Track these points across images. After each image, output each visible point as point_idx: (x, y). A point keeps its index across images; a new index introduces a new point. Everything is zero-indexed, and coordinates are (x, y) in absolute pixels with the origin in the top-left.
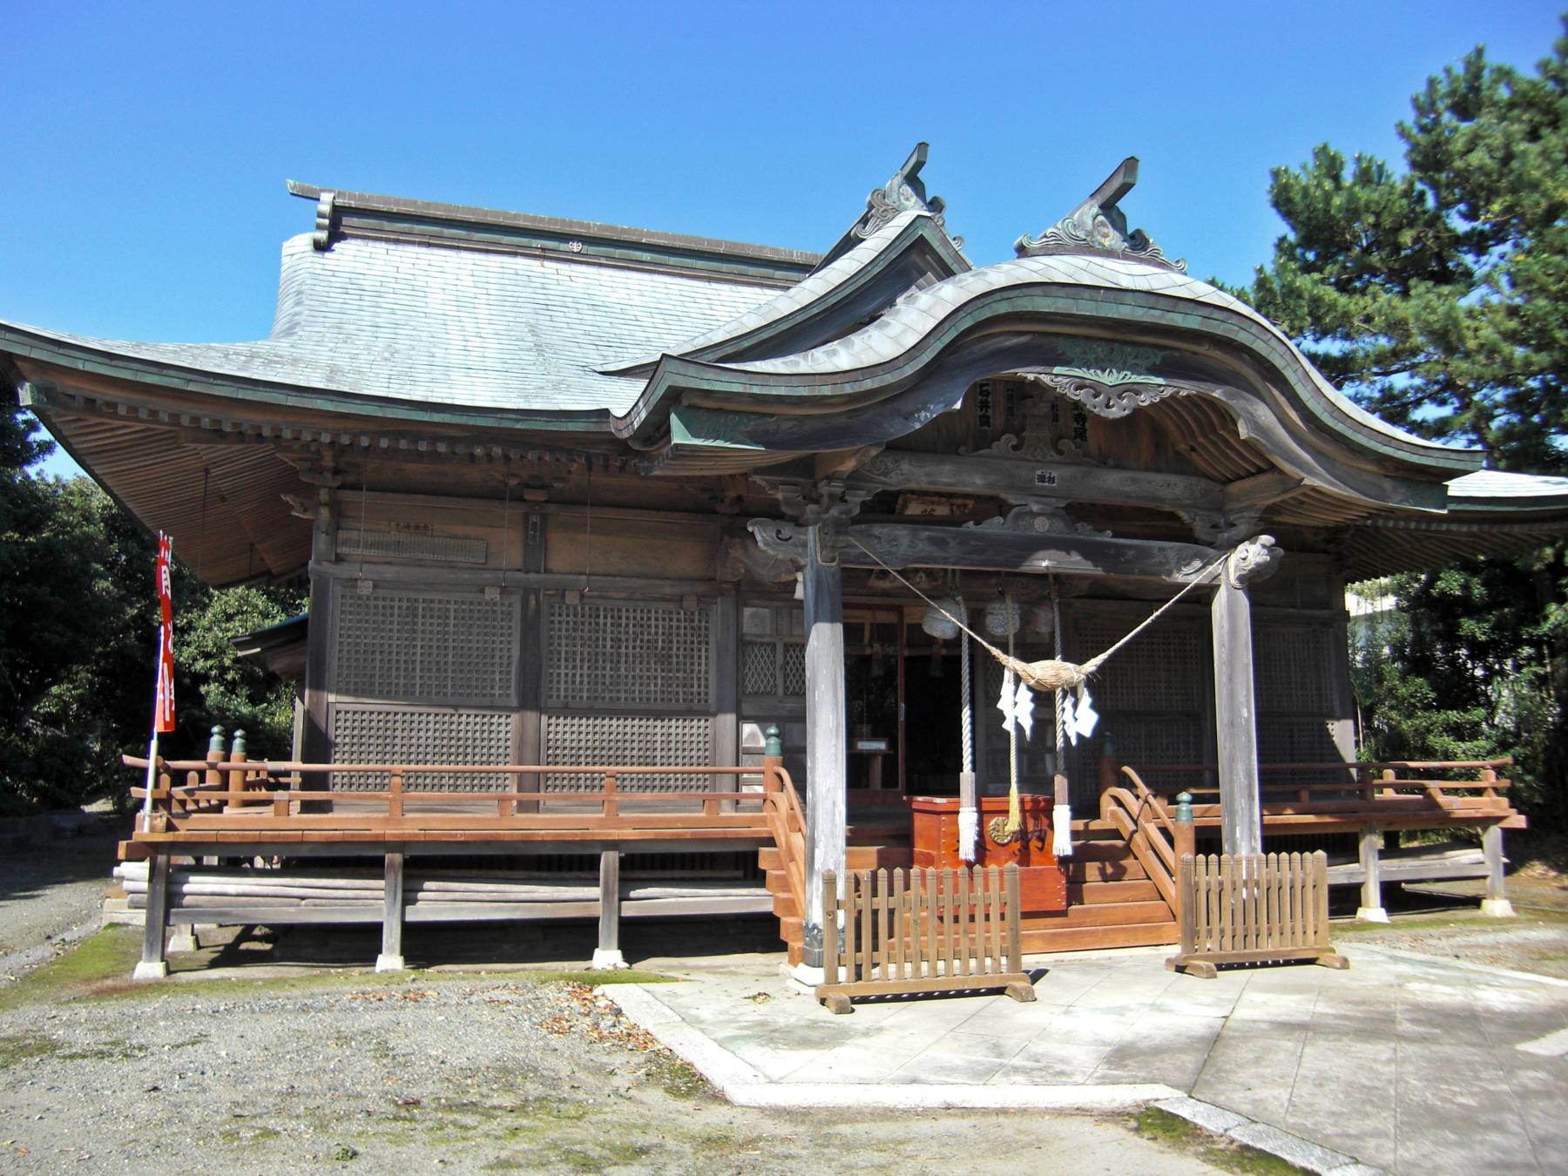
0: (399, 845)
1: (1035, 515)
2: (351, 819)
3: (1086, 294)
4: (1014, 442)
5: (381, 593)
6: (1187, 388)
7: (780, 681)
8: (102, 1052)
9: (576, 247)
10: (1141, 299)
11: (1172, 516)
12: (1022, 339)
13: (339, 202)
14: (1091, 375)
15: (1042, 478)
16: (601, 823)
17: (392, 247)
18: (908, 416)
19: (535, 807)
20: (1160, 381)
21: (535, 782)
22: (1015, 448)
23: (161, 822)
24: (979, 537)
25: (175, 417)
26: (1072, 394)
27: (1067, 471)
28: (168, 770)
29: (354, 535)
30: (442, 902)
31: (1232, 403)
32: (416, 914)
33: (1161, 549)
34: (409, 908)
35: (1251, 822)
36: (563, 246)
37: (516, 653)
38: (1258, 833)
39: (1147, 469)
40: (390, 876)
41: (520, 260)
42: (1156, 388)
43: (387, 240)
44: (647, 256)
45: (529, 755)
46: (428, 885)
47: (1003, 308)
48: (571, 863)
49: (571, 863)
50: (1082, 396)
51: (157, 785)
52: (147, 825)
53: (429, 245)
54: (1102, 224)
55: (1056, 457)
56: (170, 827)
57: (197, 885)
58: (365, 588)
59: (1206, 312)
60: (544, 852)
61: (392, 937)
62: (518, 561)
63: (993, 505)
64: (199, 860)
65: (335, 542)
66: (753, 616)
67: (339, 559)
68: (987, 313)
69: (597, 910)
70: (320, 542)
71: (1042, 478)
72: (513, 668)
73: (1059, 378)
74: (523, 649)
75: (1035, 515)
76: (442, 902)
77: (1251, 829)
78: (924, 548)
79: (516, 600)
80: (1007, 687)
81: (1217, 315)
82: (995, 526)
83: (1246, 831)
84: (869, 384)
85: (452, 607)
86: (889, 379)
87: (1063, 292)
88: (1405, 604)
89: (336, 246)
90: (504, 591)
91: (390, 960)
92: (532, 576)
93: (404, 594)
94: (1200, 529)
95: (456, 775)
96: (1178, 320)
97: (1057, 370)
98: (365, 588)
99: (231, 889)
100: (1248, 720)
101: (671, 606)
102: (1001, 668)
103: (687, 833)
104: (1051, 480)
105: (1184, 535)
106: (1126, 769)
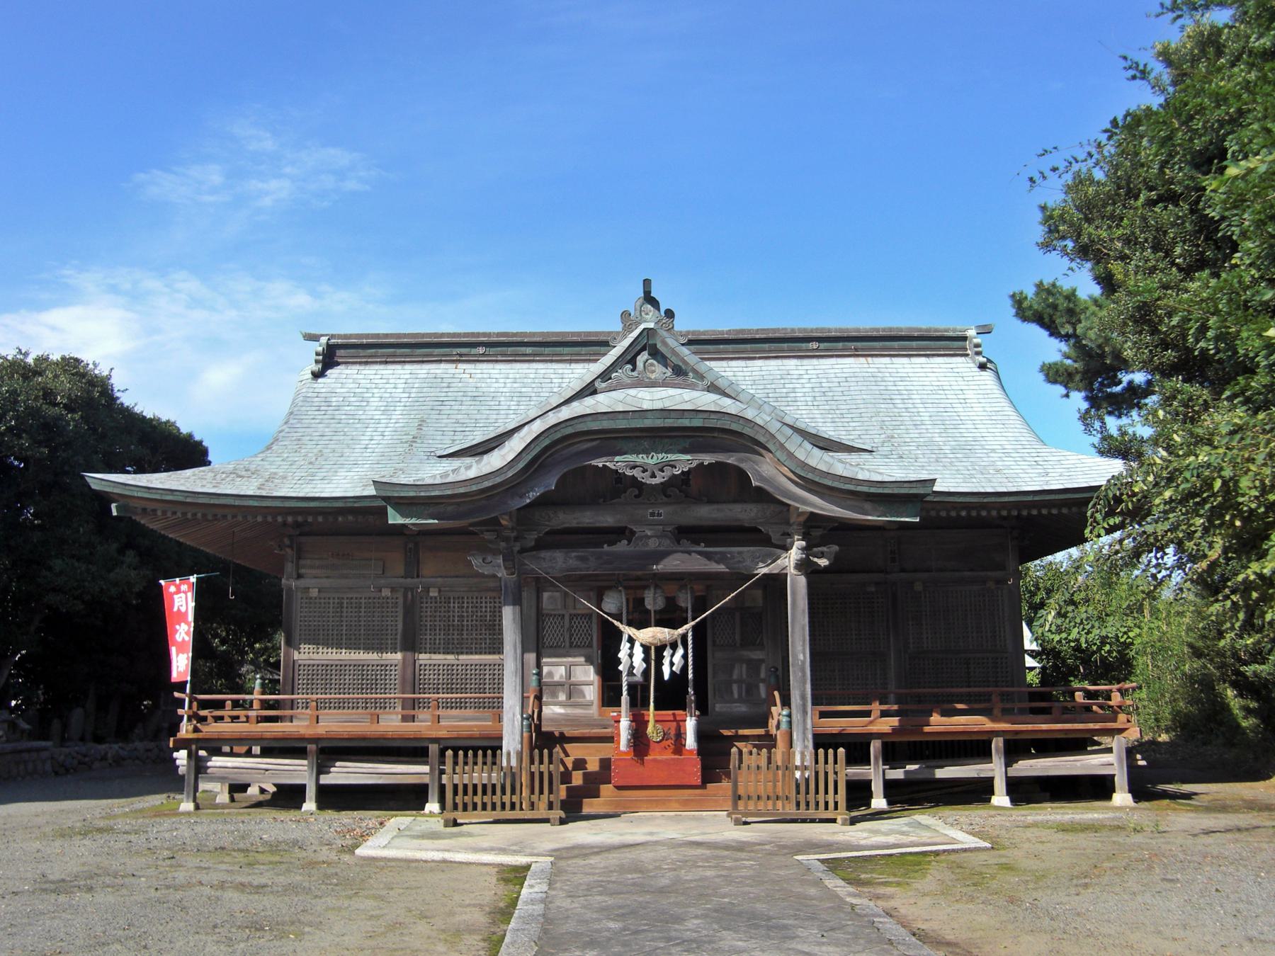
0: (315, 740)
1: (649, 537)
2: (299, 725)
5: (323, 595)
6: (708, 459)
9: (481, 350)
10: (658, 415)
11: (755, 530)
12: (594, 443)
14: (640, 459)
15: (652, 514)
16: (429, 728)
17: (362, 367)
18: (522, 496)
19: (413, 719)
20: (689, 457)
21: (414, 704)
23: (191, 728)
24: (608, 554)
26: (629, 473)
27: (670, 509)
28: (196, 699)
29: (308, 562)
30: (345, 773)
31: (743, 466)
32: (325, 780)
33: (739, 553)
34: (322, 776)
35: (805, 729)
36: (474, 351)
37: (400, 627)
39: (735, 501)
40: (310, 758)
41: (443, 366)
42: (684, 461)
43: (360, 363)
44: (529, 350)
45: (409, 688)
46: (338, 764)
47: (569, 431)
48: (412, 751)
49: (412, 751)
50: (637, 473)
51: (190, 707)
52: (185, 730)
53: (386, 362)
54: (652, 365)
56: (196, 730)
57: (217, 761)
58: (314, 593)
61: (311, 792)
62: (402, 572)
63: (620, 533)
65: (298, 567)
66: (550, 597)
67: (299, 576)
68: (558, 435)
69: (426, 780)
70: (289, 567)
71: (652, 514)
72: (399, 637)
73: (619, 463)
74: (405, 623)
75: (649, 537)
76: (345, 773)
77: (804, 733)
78: (573, 563)
79: (400, 595)
80: (625, 647)
82: (622, 546)
83: (801, 736)
84: (487, 484)
85: (363, 601)
86: (498, 480)
87: (605, 417)
90: (393, 590)
91: (310, 805)
92: (409, 580)
93: (336, 595)
94: (775, 538)
96: (686, 423)
97: (617, 458)
98: (314, 593)
99: (229, 765)
100: (803, 662)
101: (494, 594)
104: (659, 515)
105: (766, 541)
106: (776, 693)
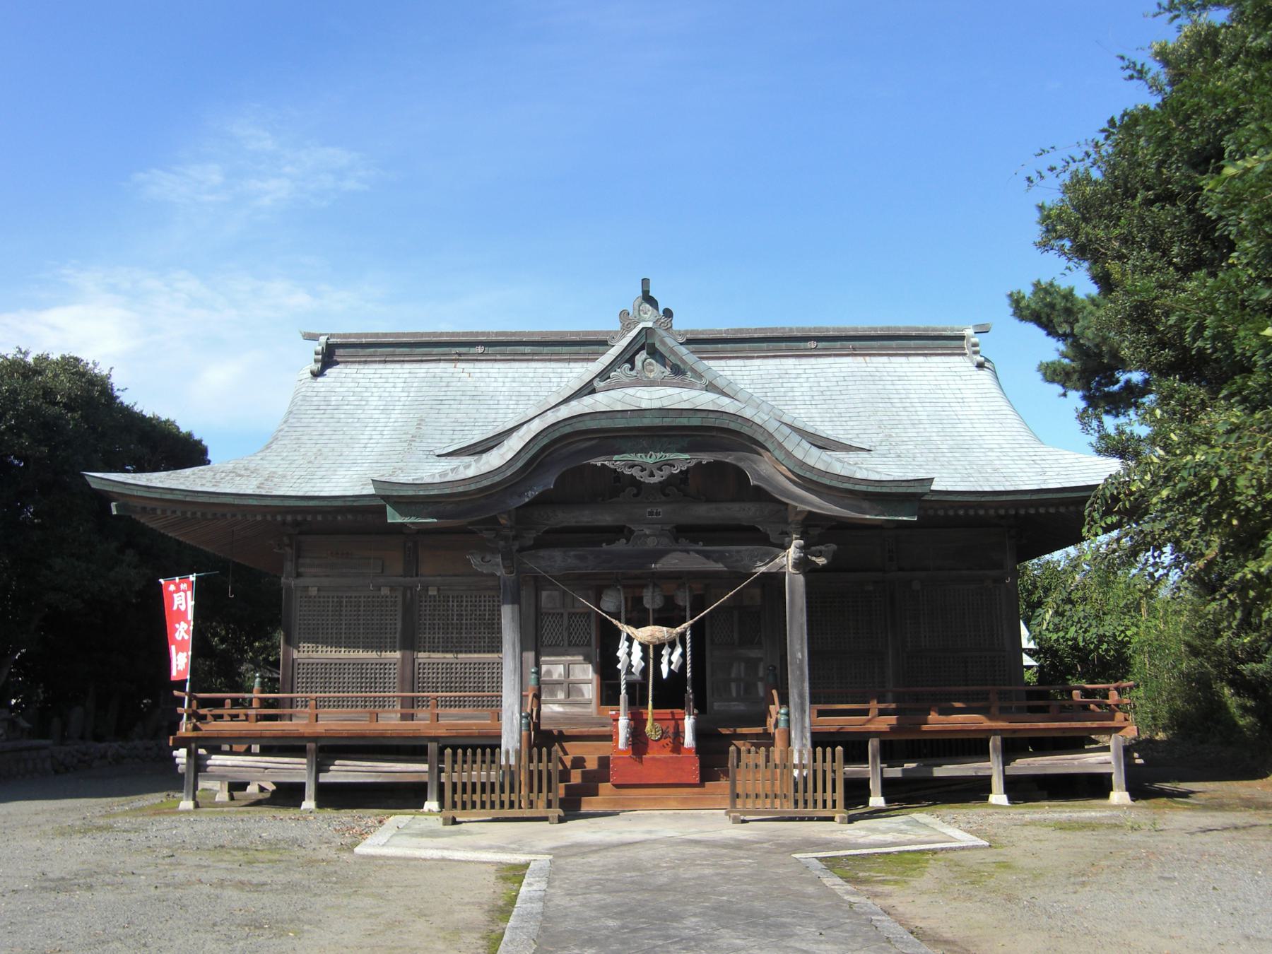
1: (648, 536)
2: (298, 724)
3: (619, 415)
4: (635, 491)
5: (322, 594)
6: (706, 458)
7: (566, 638)
8: (242, 883)
9: (480, 349)
12: (593, 442)
13: (332, 340)
14: (639, 458)
15: (651, 513)
17: (361, 366)
18: (521, 495)
19: (412, 717)
20: (687, 456)
21: (413, 702)
22: (635, 496)
23: (190, 726)
25: (184, 513)
26: (627, 472)
28: (196, 698)
29: (308, 561)
30: (344, 772)
32: (325, 778)
33: (738, 552)
34: (321, 775)
35: (803, 727)
36: (473, 350)
37: (399, 626)
38: (808, 735)
41: (442, 365)
42: (683, 460)
44: (528, 349)
45: (408, 687)
48: (410, 749)
49: (410, 749)
50: (635, 472)
51: (190, 706)
54: (650, 364)
55: (664, 498)
56: (196, 728)
57: (216, 760)
58: (313, 592)
59: (704, 415)
60: (395, 743)
61: (310, 791)
63: (619, 532)
64: (250, 748)
67: (299, 575)
68: (557, 434)
69: (425, 778)
71: (651, 513)
73: (617, 462)
75: (648, 536)
76: (344, 772)
81: (711, 415)
82: (620, 545)
84: (486, 483)
87: (604, 416)
88: (280, 637)
89: (328, 371)
90: (392, 589)
91: (309, 804)
92: (408, 579)
94: (774, 537)
95: (365, 699)
97: (616, 457)
98: (313, 592)
99: (229, 763)
100: (801, 661)
102: (619, 632)
103: (475, 731)
104: (658, 514)
105: (764, 540)
106: (774, 692)
